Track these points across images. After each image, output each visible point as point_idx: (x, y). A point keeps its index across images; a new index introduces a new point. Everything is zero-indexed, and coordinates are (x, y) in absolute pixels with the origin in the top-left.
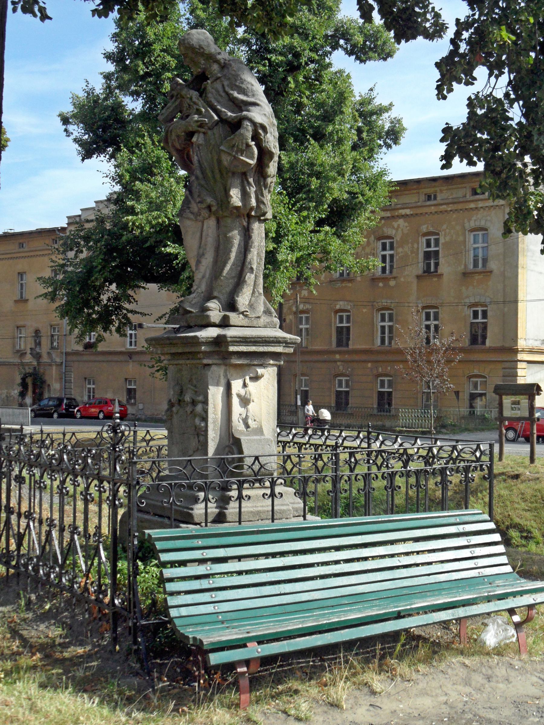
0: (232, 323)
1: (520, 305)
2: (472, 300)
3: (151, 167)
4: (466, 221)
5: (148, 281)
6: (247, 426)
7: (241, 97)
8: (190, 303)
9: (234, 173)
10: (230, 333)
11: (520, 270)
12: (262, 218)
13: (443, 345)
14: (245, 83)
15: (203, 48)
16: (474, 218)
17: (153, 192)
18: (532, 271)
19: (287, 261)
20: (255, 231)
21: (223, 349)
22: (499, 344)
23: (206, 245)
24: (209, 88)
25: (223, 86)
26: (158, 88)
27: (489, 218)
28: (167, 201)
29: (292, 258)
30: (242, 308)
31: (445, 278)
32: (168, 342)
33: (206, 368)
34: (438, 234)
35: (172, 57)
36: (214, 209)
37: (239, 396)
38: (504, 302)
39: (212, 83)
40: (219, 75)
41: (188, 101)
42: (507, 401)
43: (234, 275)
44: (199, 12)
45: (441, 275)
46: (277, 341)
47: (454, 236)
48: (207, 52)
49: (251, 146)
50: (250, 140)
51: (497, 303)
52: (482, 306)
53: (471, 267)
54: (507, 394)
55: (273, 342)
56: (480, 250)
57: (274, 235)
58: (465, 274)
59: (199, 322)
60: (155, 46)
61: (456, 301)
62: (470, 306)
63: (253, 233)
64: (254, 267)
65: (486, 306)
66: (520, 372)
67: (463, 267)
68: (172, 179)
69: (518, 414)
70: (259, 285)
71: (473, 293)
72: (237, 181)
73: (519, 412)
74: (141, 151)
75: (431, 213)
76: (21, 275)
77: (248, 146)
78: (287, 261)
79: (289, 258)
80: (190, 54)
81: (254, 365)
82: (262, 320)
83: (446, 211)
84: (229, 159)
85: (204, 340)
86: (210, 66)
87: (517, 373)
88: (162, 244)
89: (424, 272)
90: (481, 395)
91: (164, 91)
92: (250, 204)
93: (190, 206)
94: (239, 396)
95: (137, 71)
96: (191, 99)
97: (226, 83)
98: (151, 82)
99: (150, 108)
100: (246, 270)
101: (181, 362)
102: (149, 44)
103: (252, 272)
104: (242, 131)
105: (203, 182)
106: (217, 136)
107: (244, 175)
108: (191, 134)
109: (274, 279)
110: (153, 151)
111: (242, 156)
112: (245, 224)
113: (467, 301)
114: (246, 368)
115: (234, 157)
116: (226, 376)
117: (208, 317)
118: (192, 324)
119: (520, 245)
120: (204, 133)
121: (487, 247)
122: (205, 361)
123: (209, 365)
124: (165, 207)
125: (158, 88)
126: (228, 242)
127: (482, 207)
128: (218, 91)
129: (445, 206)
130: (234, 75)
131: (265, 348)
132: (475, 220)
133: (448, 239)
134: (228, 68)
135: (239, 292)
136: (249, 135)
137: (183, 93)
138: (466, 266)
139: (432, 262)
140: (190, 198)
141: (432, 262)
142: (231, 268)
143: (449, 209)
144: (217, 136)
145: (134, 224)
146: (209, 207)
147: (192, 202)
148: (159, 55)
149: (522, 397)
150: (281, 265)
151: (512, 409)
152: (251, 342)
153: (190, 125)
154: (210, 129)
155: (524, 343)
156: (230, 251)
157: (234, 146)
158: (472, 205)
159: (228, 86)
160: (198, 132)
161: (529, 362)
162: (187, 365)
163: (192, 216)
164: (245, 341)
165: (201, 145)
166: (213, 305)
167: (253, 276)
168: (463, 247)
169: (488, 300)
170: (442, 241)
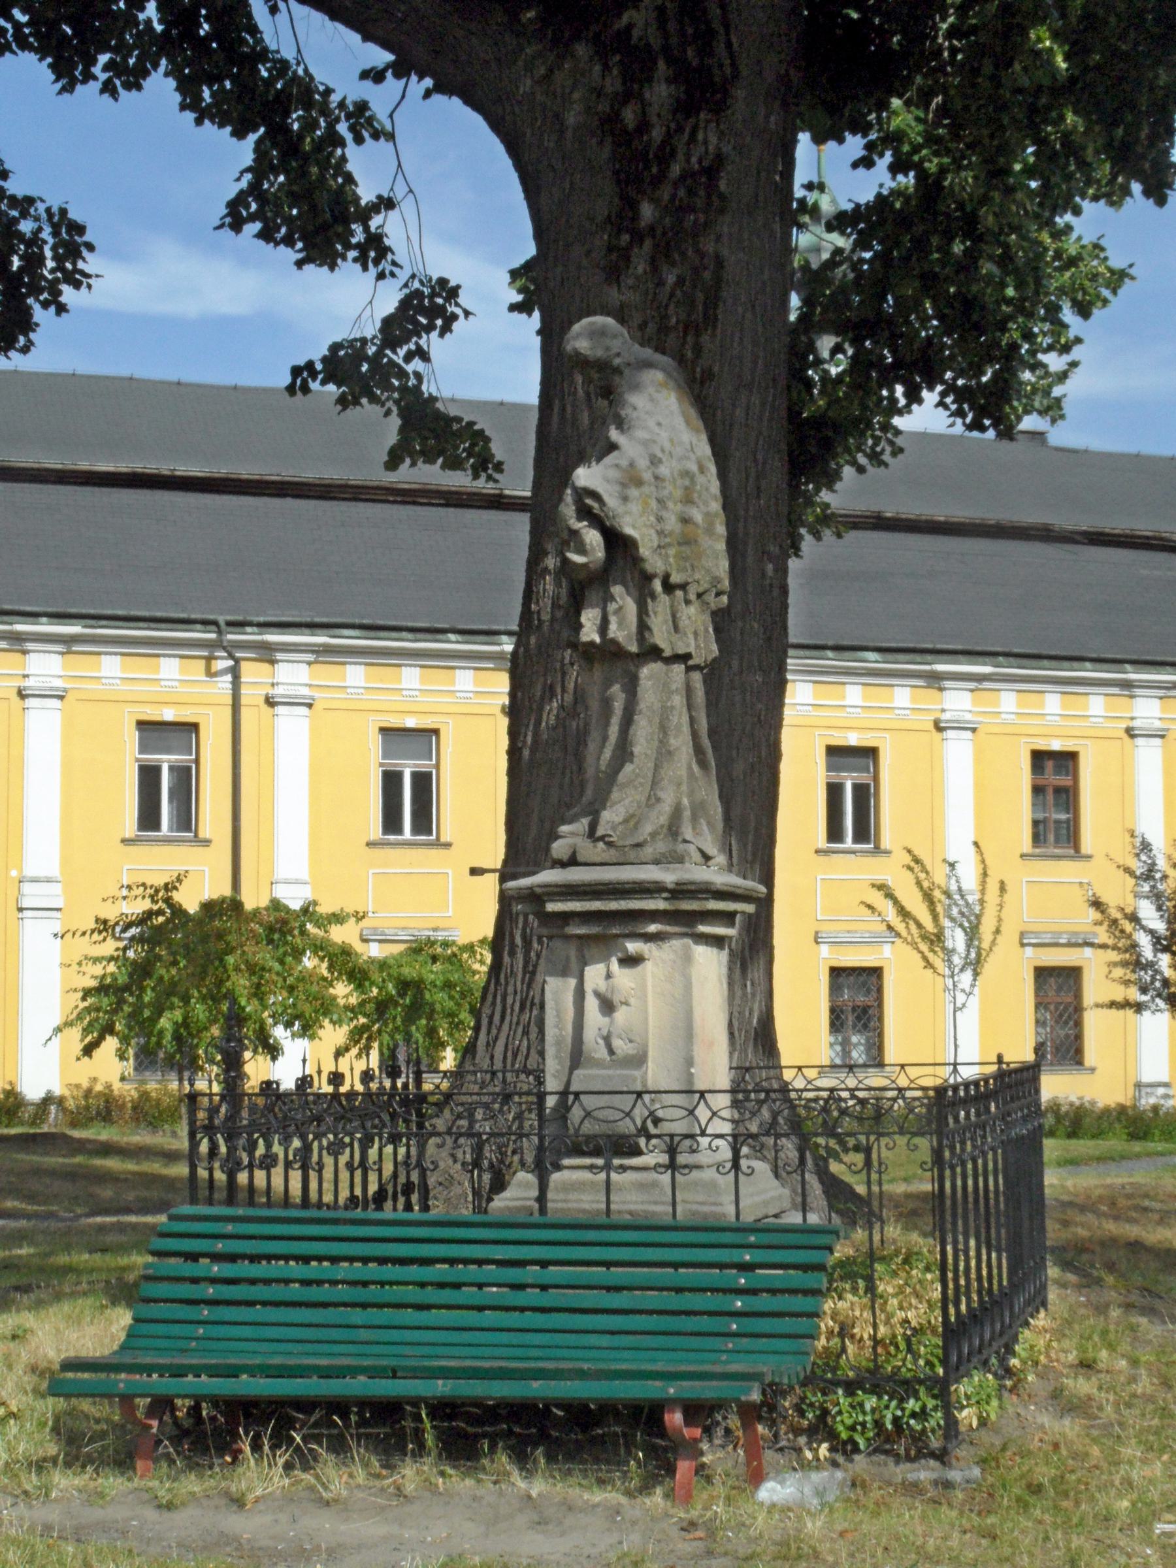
6: (611, 1052)
37: (597, 994)
76: (270, 702)
81: (617, 936)
94: (597, 994)
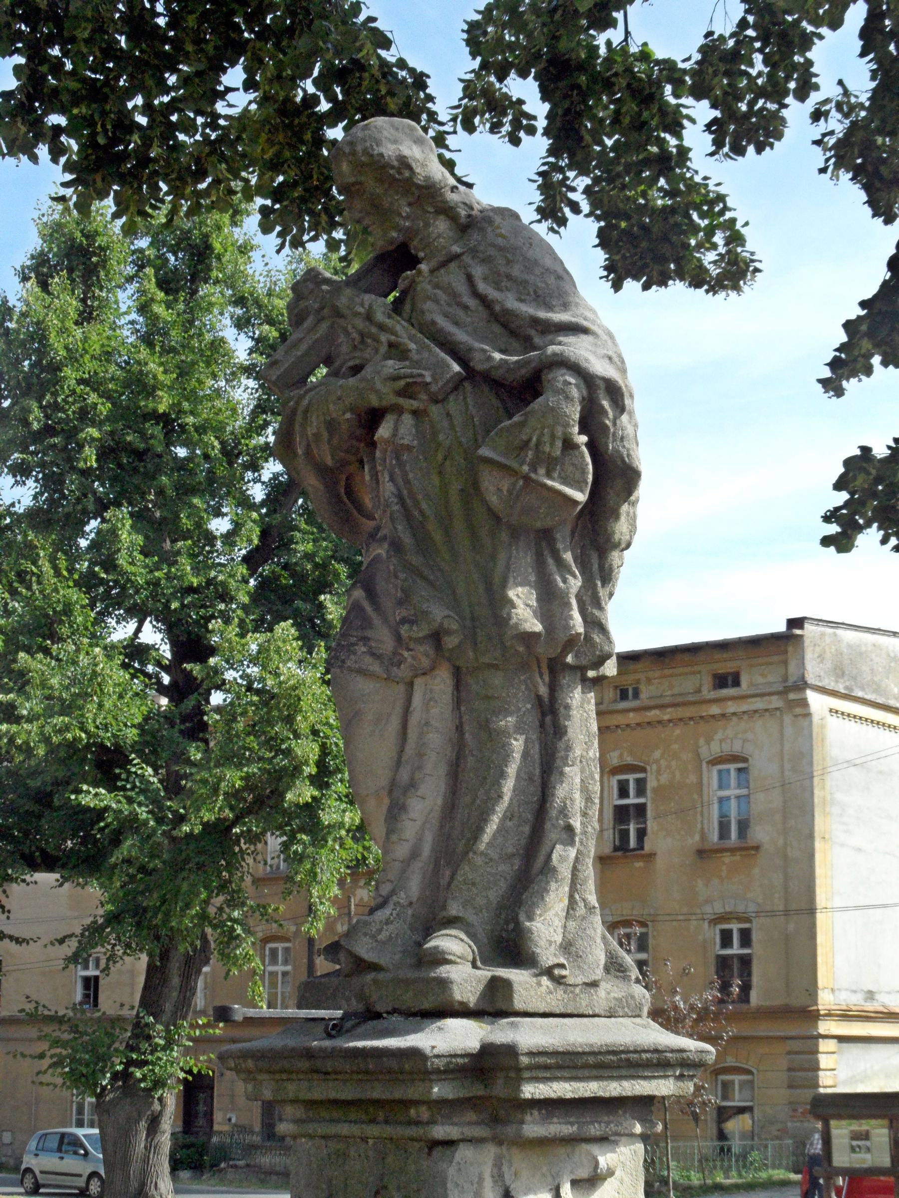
0: (519, 1004)
1: (820, 918)
2: (719, 908)
3: (52, 624)
4: (702, 741)
5: (34, 866)
7: (528, 309)
8: (374, 937)
9: (515, 533)
10: (528, 1036)
11: (818, 845)
12: (591, 674)
13: (692, 1008)
14: (537, 271)
15: (410, 168)
16: (719, 736)
17: (53, 676)
18: (842, 845)
19: (341, 825)
20: (574, 712)
21: (500, 1090)
22: (778, 1001)
23: (420, 755)
24: (424, 286)
25: (470, 279)
26: (70, 460)
27: (750, 736)
28: (85, 695)
29: (352, 819)
30: (548, 956)
31: (660, 863)
32: (304, 1064)
33: (437, 1152)
34: (643, 770)
35: (100, 396)
36: (451, 642)
38: (787, 913)
39: (432, 271)
40: (456, 249)
41: (360, 323)
42: (841, 1131)
43: (511, 850)
44: (159, 309)
45: (652, 856)
46: (657, 1062)
47: (678, 774)
48: (419, 180)
49: (576, 447)
50: (576, 429)
51: (771, 914)
52: (740, 919)
53: (715, 837)
54: (840, 1117)
55: (648, 1065)
56: (733, 803)
57: (314, 771)
58: (702, 853)
59: (409, 1000)
60: (67, 371)
61: (685, 910)
62: (714, 921)
63: (568, 718)
64: (576, 823)
65: (748, 920)
66: (824, 1061)
67: (697, 837)
68: (97, 650)
69: (864, 1160)
70: (585, 880)
71: (721, 892)
72: (524, 560)
73: (868, 1156)
74: (29, 588)
75: (627, 725)
77: (569, 445)
78: (341, 825)
79: (347, 819)
80: (370, 183)
82: (602, 992)
83: (659, 722)
84: (505, 485)
85: (440, 1063)
86: (427, 225)
87: (817, 1062)
88: (71, 788)
89: (616, 849)
90: (741, 1110)
91: (81, 465)
92: (568, 627)
93: (369, 633)
95: (26, 423)
96: (369, 317)
97: (478, 271)
98: (55, 445)
99: (51, 501)
100: (552, 835)
101: (344, 1129)
102: (55, 368)
103: (572, 843)
104: (549, 399)
105: (416, 560)
106: (458, 420)
107: (545, 539)
108: (372, 418)
109: (314, 865)
110: (56, 590)
111: (549, 475)
112: (543, 690)
113: (708, 909)
114: (562, 1151)
115: (526, 478)
116: (499, 1177)
117: (444, 984)
118: (380, 1008)
119: (817, 792)
120: (415, 413)
121: (748, 796)
122: (440, 1132)
123: (449, 1144)
124: (81, 708)
125: (69, 457)
126: (494, 742)
127: (734, 714)
128: (454, 295)
129: (657, 712)
130: (501, 249)
131: (626, 1084)
132: (721, 741)
133: (664, 778)
134: (482, 230)
135: (534, 905)
136: (574, 412)
137: (342, 302)
138: (703, 836)
139: (632, 828)
140: (368, 609)
141: (632, 828)
142: (501, 829)
143: (666, 717)
144: (458, 420)
145: (12, 740)
146: (436, 637)
147: (377, 620)
148: (74, 392)
149: (873, 1122)
150: (329, 833)
151: (853, 1149)
152: (586, 1066)
153: (373, 390)
154: (435, 400)
155: (831, 997)
156: (502, 775)
157: (526, 444)
158: (715, 710)
159: (485, 279)
160: (398, 410)
161: (842, 1039)
162: (364, 1140)
163: (376, 667)
164: (569, 1063)
165: (409, 448)
166: (452, 943)
167: (572, 853)
168: (696, 796)
169: (752, 908)
170: (651, 784)
